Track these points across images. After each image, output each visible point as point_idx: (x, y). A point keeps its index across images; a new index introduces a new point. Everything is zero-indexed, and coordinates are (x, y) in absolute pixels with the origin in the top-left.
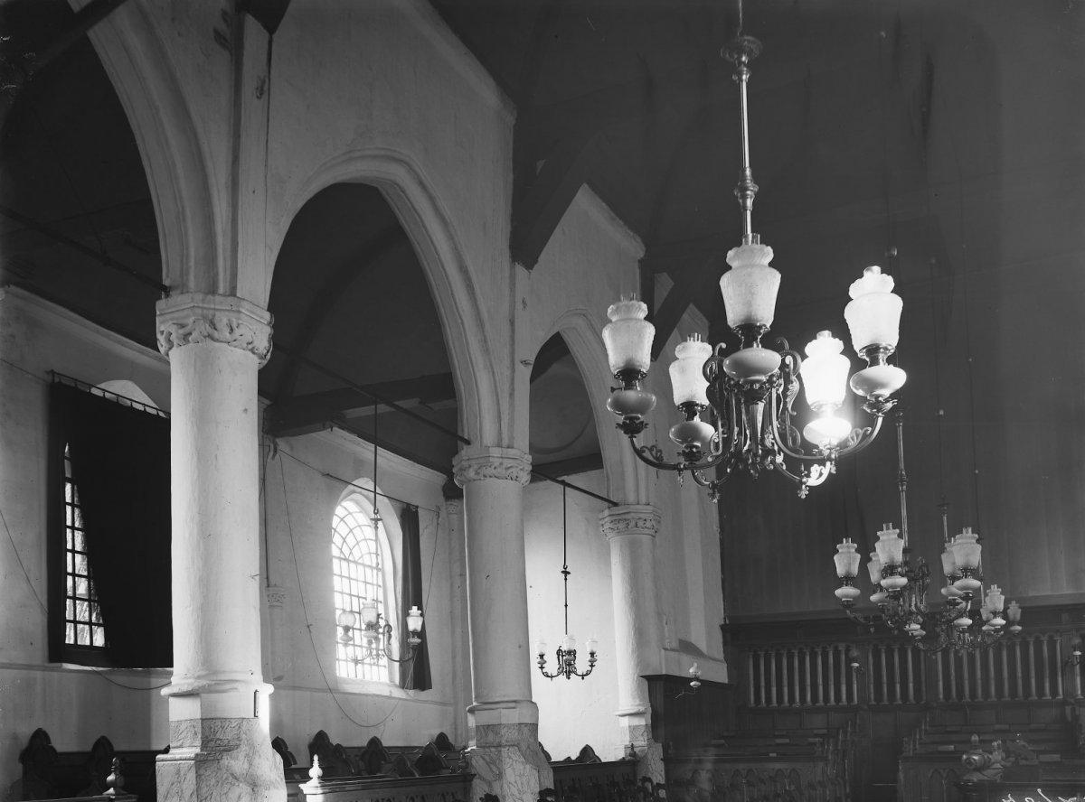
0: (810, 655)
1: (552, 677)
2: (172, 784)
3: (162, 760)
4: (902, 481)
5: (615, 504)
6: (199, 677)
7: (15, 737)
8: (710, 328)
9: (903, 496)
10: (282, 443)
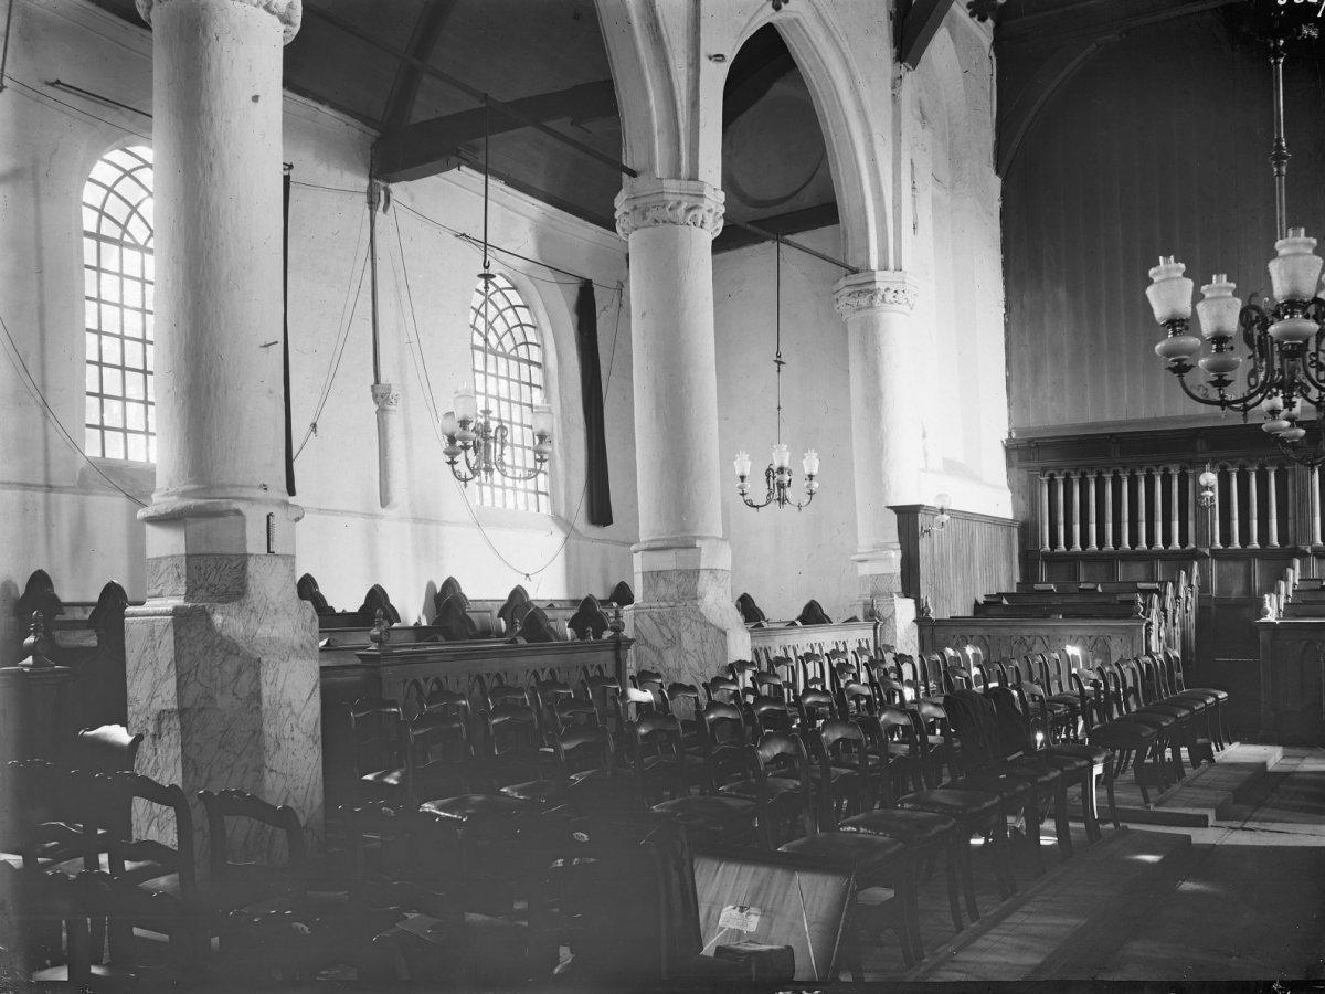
1: (758, 507)
2: (145, 651)
3: (133, 615)
4: (1279, 158)
5: (855, 271)
6: (184, 495)
7: (431, 585)
10: (397, 189)
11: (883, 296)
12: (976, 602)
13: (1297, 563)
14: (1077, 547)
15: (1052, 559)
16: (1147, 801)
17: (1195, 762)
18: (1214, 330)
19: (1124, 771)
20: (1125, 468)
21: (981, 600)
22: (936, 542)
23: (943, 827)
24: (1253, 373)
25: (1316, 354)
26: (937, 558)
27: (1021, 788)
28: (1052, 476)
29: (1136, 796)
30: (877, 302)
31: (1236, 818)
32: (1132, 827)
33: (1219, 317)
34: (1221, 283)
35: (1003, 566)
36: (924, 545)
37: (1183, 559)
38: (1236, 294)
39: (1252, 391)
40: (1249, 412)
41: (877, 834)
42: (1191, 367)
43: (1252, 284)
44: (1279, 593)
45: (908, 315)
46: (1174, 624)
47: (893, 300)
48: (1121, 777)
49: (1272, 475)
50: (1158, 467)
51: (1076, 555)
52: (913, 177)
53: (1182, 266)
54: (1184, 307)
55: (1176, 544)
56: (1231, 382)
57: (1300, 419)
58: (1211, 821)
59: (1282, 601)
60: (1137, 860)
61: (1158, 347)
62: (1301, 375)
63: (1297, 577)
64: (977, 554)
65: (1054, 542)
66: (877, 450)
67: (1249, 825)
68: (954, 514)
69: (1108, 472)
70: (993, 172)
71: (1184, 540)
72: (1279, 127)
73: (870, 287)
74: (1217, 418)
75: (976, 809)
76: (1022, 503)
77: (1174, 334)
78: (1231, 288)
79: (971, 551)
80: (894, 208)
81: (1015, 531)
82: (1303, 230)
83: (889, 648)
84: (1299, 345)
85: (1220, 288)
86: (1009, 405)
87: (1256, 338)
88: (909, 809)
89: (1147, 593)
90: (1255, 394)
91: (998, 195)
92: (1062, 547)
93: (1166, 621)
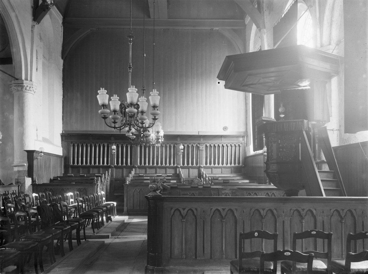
0: (86, 147)
4: (130, 68)
5: (17, 79)
8: (63, 19)
9: (130, 74)
11: (26, 88)
12: (51, 179)
13: (134, 169)
14: (80, 164)
15: (73, 167)
16: (94, 232)
17: (107, 221)
18: (114, 109)
19: (89, 225)
20: (85, 143)
21: (52, 178)
22: (39, 161)
23: (33, 245)
24: (122, 121)
25: (137, 118)
26: (39, 166)
27: (59, 232)
28: (74, 144)
29: (91, 231)
30: (24, 90)
31: (116, 235)
32: (89, 240)
33: (115, 105)
34: (115, 98)
35: (59, 169)
36: (35, 162)
37: (107, 168)
38: (119, 100)
39: (122, 125)
40: (121, 130)
41: (12, 249)
42: (107, 117)
43: (123, 98)
44: (129, 177)
45: (34, 95)
46: (104, 185)
47: (29, 89)
48: (88, 226)
49: (129, 147)
50: (97, 143)
51: (80, 166)
52: (37, 55)
53: (106, 91)
54: (106, 102)
55: (105, 164)
56: (117, 122)
57: (134, 134)
58: (110, 237)
59: (130, 179)
60: (298, 89)
61: (99, 111)
62: (133, 122)
63: (134, 173)
64: (51, 165)
65: (74, 162)
66: (22, 135)
67: (119, 237)
68: (45, 153)
69: (76, 144)
70: (61, 58)
71: (107, 163)
72: (130, 60)
73: (22, 85)
74: (113, 131)
75: (44, 239)
76: (65, 151)
77: (104, 108)
78: (118, 99)
79: (50, 165)
80: (30, 63)
81: (63, 159)
82: (134, 86)
83: (23, 193)
84: (133, 115)
85: (115, 98)
86: (63, 123)
87: (123, 112)
88: (23, 241)
89: (97, 176)
90: (122, 126)
91: (62, 65)
92: (76, 164)
93: (102, 184)
